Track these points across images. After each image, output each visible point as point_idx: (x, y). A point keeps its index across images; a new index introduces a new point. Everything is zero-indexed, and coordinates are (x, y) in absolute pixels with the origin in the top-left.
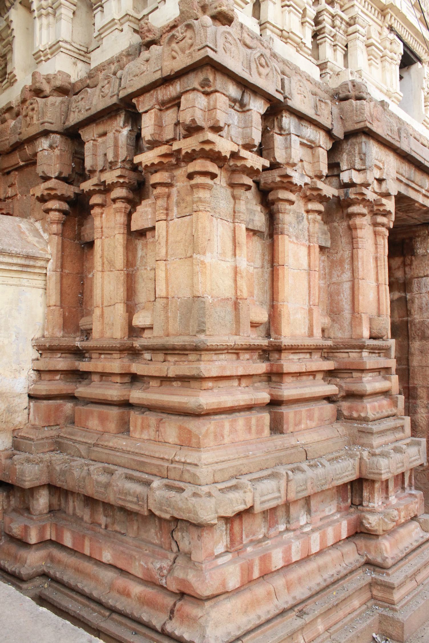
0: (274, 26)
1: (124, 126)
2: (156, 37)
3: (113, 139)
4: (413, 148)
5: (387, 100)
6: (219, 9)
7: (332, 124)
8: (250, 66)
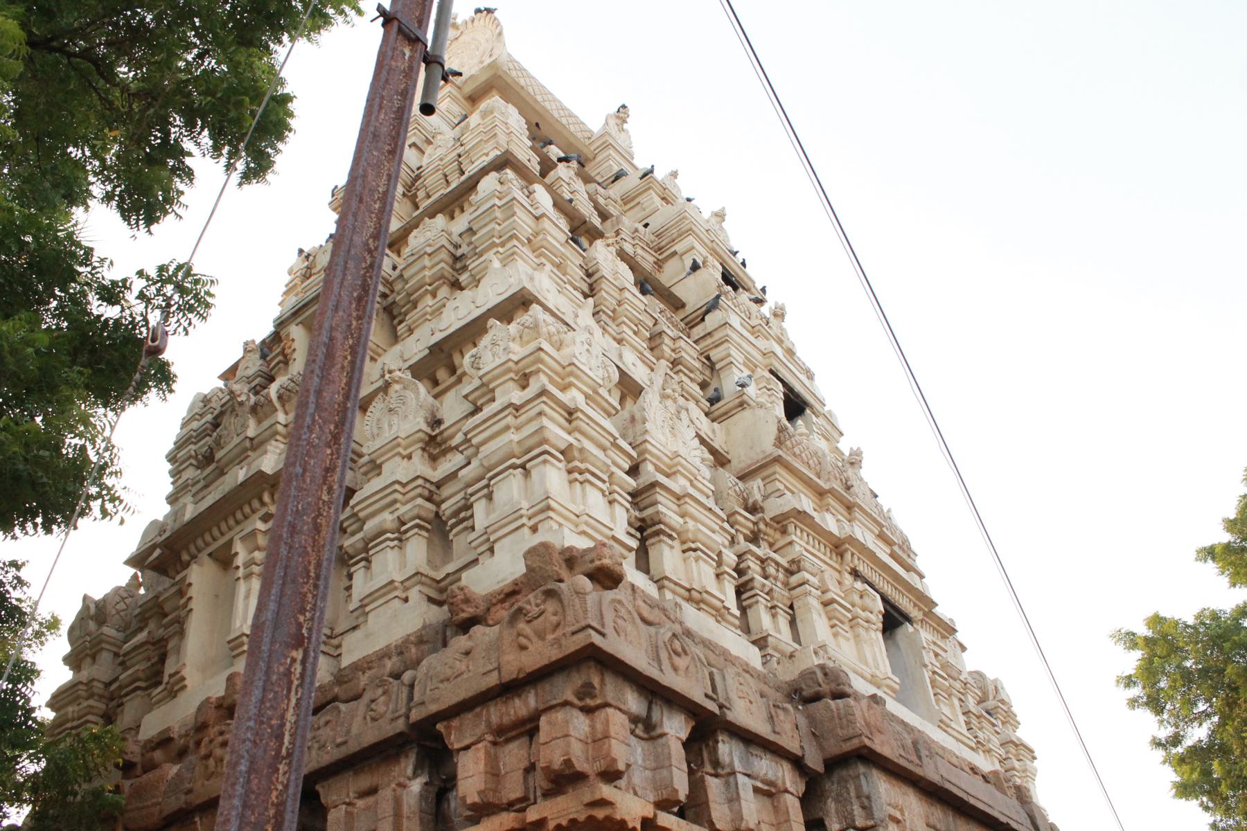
0: (676, 584)
1: (415, 775)
2: (479, 612)
3: (391, 803)
4: (945, 775)
5: (880, 693)
6: (598, 563)
7: (802, 747)
8: (658, 655)
